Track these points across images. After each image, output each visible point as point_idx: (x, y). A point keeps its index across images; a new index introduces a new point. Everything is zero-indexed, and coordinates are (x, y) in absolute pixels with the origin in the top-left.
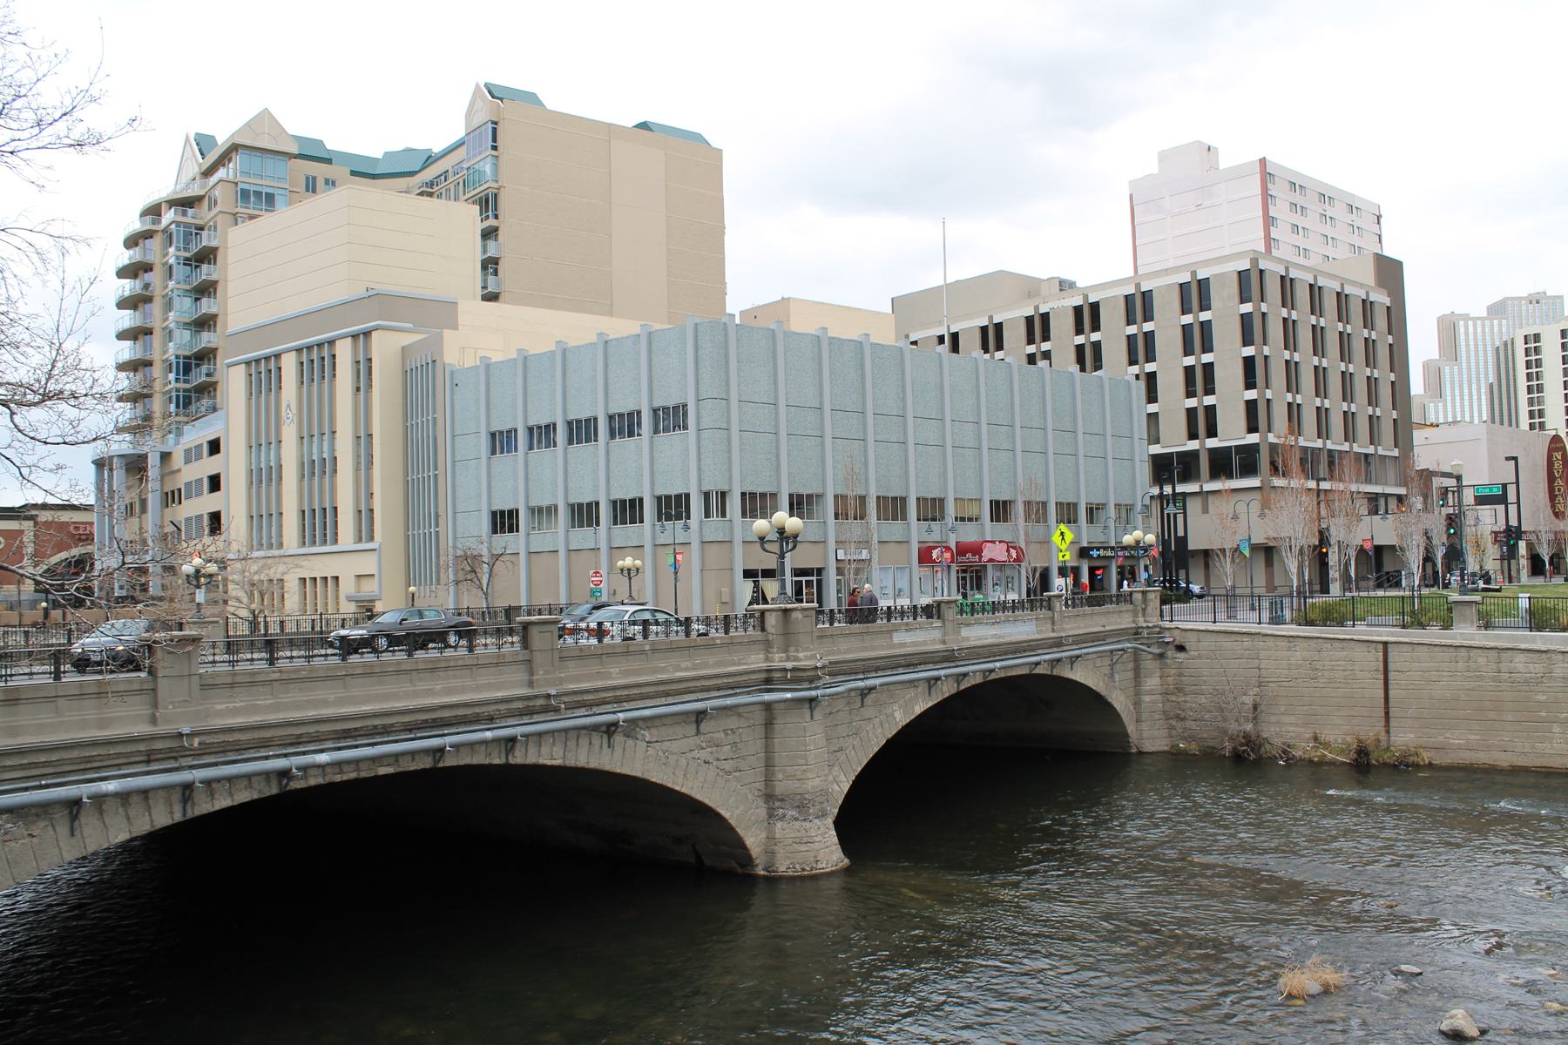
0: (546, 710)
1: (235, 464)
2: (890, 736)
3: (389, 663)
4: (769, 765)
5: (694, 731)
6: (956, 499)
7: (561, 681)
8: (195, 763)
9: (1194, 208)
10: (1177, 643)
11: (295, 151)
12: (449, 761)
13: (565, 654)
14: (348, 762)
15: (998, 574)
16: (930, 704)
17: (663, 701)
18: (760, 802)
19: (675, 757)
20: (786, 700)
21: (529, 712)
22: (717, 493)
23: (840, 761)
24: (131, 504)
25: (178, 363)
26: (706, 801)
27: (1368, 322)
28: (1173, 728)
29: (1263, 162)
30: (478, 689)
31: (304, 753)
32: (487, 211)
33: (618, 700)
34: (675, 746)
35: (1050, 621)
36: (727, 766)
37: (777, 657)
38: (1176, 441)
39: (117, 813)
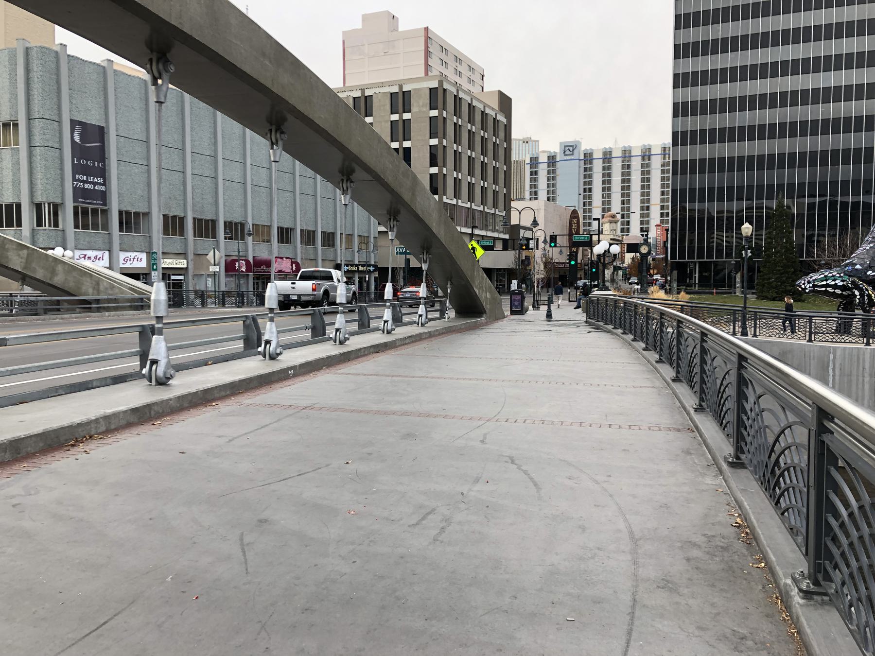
9: (383, 54)
22: (49, 205)
29: (427, 29)
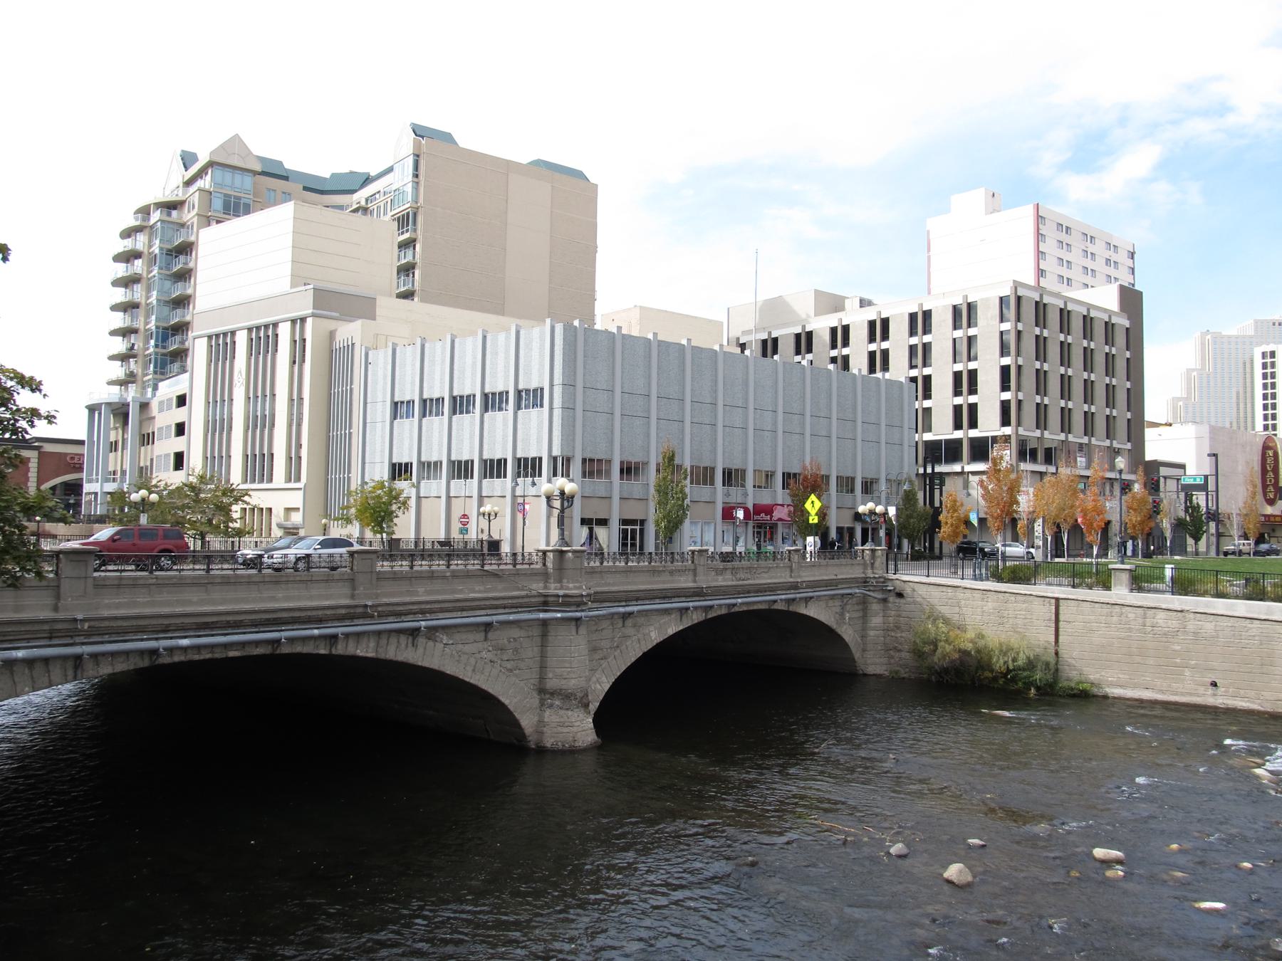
0: (365, 616)
1: (196, 416)
2: (646, 650)
3: (242, 576)
4: (543, 667)
5: (483, 638)
6: (755, 471)
7: (377, 596)
8: (86, 641)
10: (897, 591)
11: (258, 168)
12: (286, 650)
13: (381, 576)
14: (205, 646)
15: (787, 530)
16: (681, 628)
17: (459, 614)
18: (535, 694)
19: (466, 656)
20: (557, 619)
21: (351, 617)
23: (603, 666)
24: (116, 442)
25: (157, 332)
26: (491, 691)
27: (1109, 340)
28: (892, 657)
30: (311, 598)
31: (171, 638)
32: (408, 225)
33: (423, 612)
34: (467, 648)
35: (788, 570)
36: (509, 665)
37: (553, 586)
38: (942, 430)
39: (44, 676)
